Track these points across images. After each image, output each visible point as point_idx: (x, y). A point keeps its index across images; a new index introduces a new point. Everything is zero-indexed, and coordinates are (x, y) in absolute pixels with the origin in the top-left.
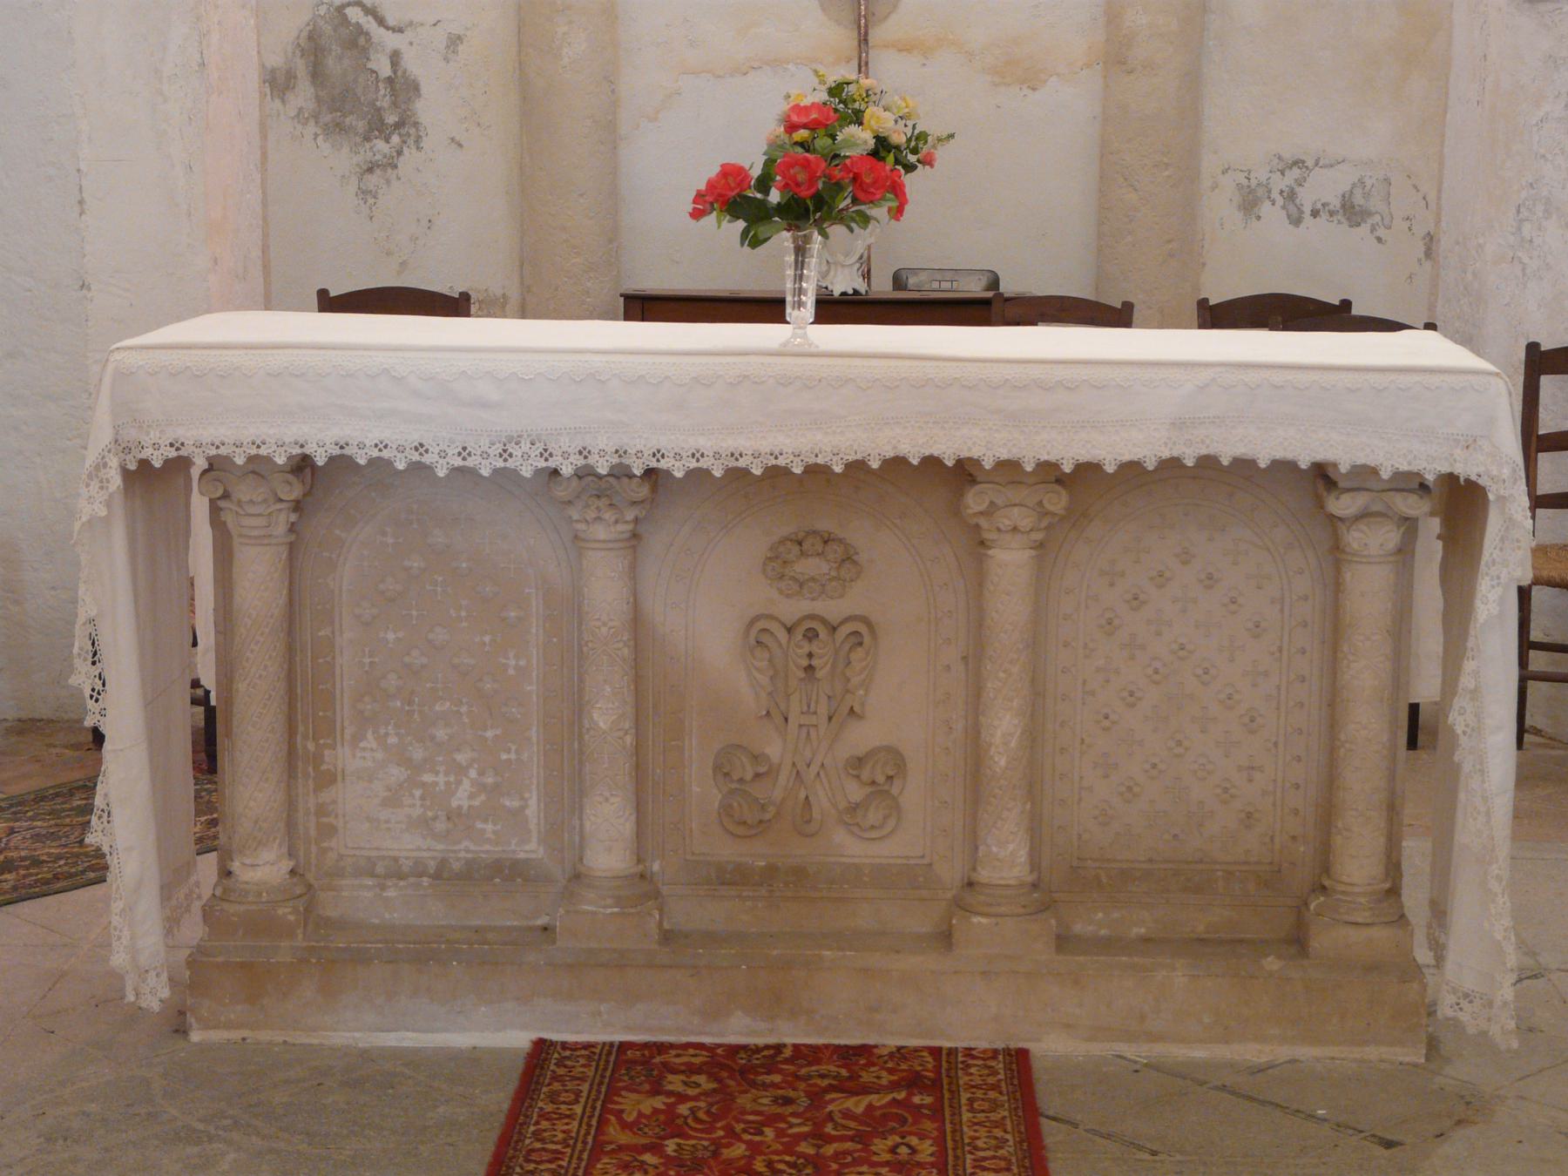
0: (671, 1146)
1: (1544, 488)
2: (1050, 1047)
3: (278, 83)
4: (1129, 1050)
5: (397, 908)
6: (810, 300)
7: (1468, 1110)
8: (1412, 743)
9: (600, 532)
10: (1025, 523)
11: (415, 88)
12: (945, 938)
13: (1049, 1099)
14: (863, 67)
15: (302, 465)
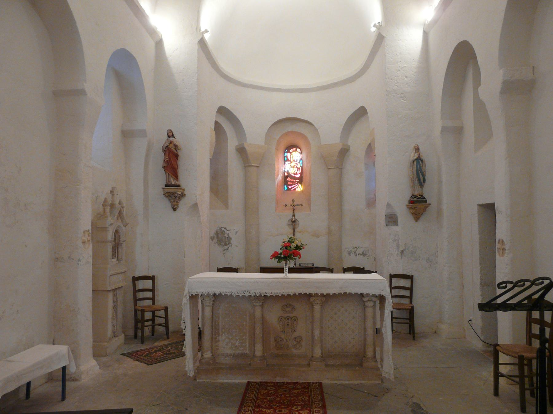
0: (268, 398)
1: (393, 295)
2: (325, 382)
3: (212, 238)
4: (337, 382)
5: (227, 361)
6: (287, 268)
7: (387, 391)
8: (377, 333)
9: (257, 304)
10: (319, 302)
11: (231, 239)
12: (309, 365)
13: (325, 390)
14: (294, 235)
15: (215, 295)
